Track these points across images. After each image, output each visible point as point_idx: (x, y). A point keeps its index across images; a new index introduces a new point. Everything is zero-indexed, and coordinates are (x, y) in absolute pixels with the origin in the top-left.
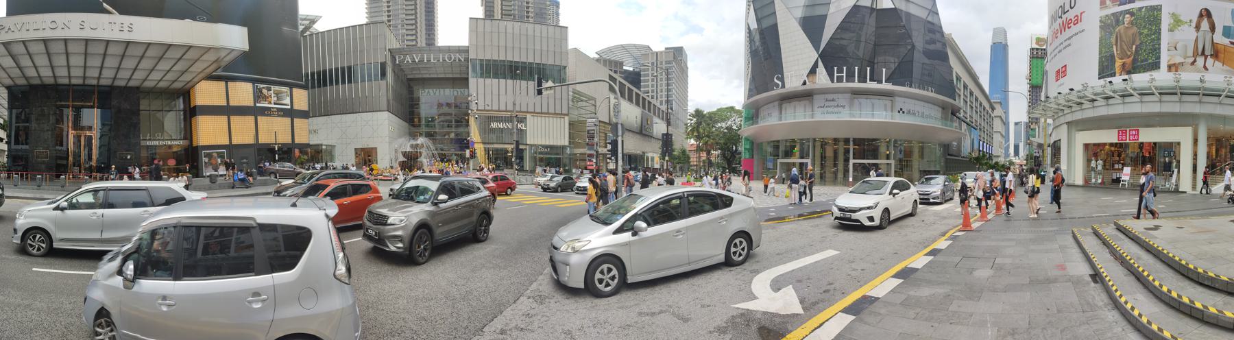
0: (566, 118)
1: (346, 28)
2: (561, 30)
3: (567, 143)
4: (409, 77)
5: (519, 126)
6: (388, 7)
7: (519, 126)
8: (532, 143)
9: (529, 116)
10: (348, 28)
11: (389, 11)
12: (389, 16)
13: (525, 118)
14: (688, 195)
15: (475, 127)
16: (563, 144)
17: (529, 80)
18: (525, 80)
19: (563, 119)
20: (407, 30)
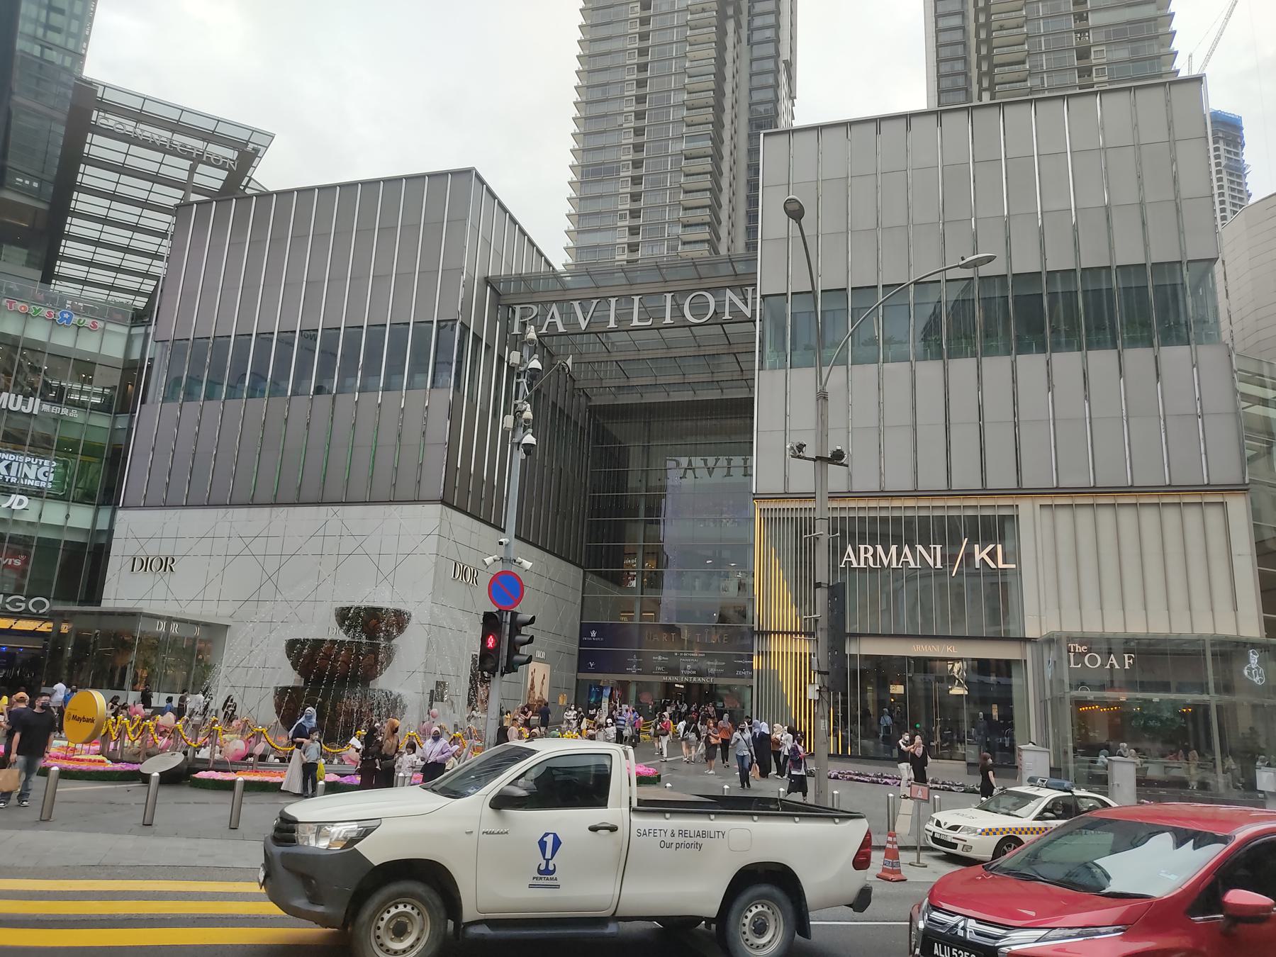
0: (1238, 507)
1: (322, 189)
2: (143, 804)
3: (1251, 626)
4: (597, 401)
5: (980, 554)
6: (635, 197)
7: (980, 554)
8: (1051, 626)
9: (1027, 509)
10: (305, 192)
11: (635, 214)
12: (634, 231)
13: (1013, 519)
14: (45, 304)
15: (775, 562)
16: (1226, 629)
17: (1023, 349)
18: (1069, 347)
19: (1214, 515)
20: (685, 226)
